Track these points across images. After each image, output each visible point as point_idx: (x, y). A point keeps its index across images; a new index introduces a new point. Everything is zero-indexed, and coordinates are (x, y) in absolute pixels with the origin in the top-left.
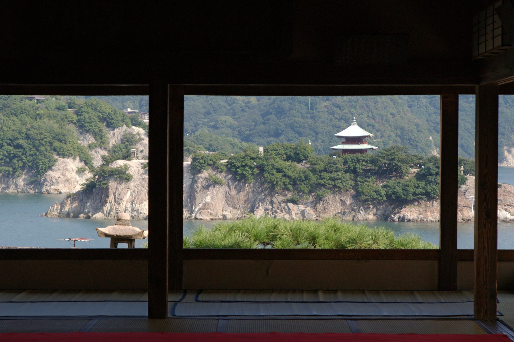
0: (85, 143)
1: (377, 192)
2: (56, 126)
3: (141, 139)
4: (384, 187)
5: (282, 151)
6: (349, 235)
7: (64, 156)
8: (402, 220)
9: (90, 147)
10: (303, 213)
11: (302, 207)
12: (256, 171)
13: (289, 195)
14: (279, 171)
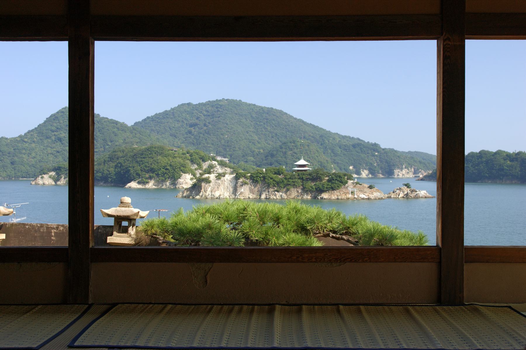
0: (194, 168)
1: (312, 187)
2: (182, 161)
3: (216, 166)
4: (314, 185)
5: (272, 171)
6: (308, 216)
7: (185, 173)
8: (322, 198)
9: (196, 169)
10: (281, 196)
11: (281, 193)
12: (262, 179)
13: (276, 189)
14: (271, 178)
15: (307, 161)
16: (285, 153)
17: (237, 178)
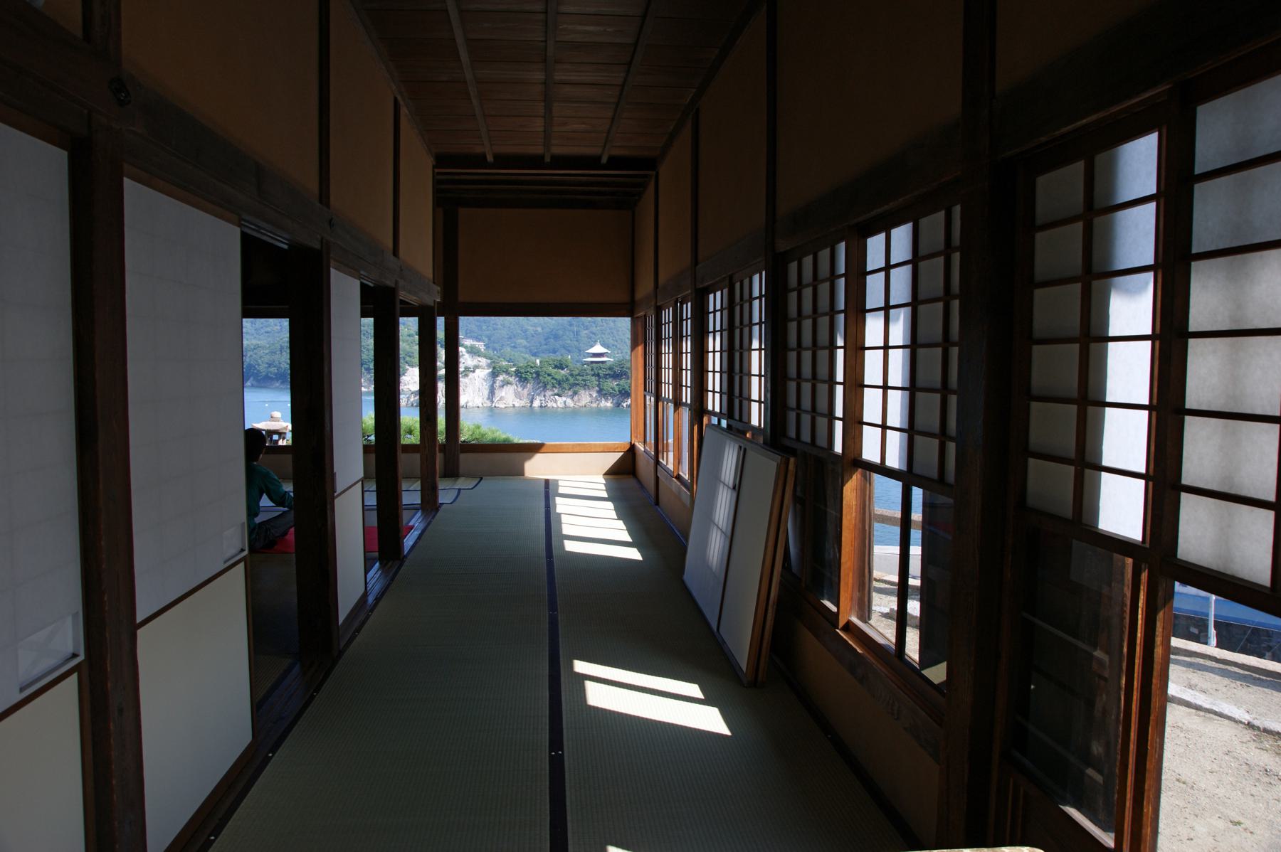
15: (607, 347)
16: (577, 333)
17: (494, 374)
